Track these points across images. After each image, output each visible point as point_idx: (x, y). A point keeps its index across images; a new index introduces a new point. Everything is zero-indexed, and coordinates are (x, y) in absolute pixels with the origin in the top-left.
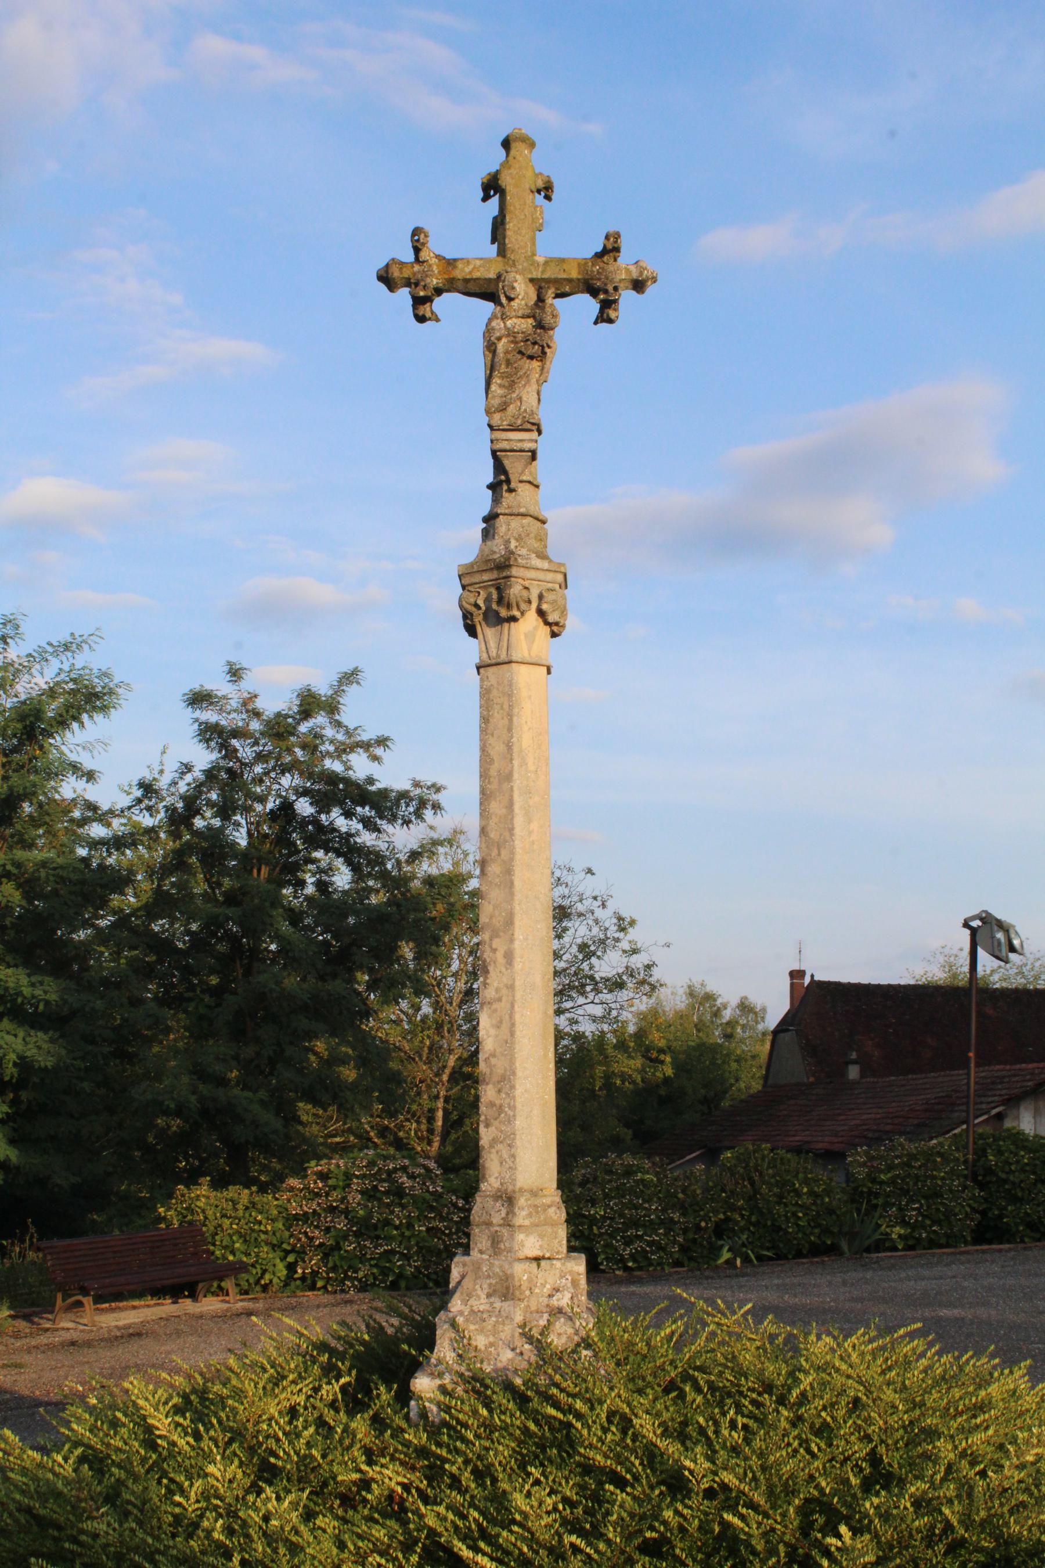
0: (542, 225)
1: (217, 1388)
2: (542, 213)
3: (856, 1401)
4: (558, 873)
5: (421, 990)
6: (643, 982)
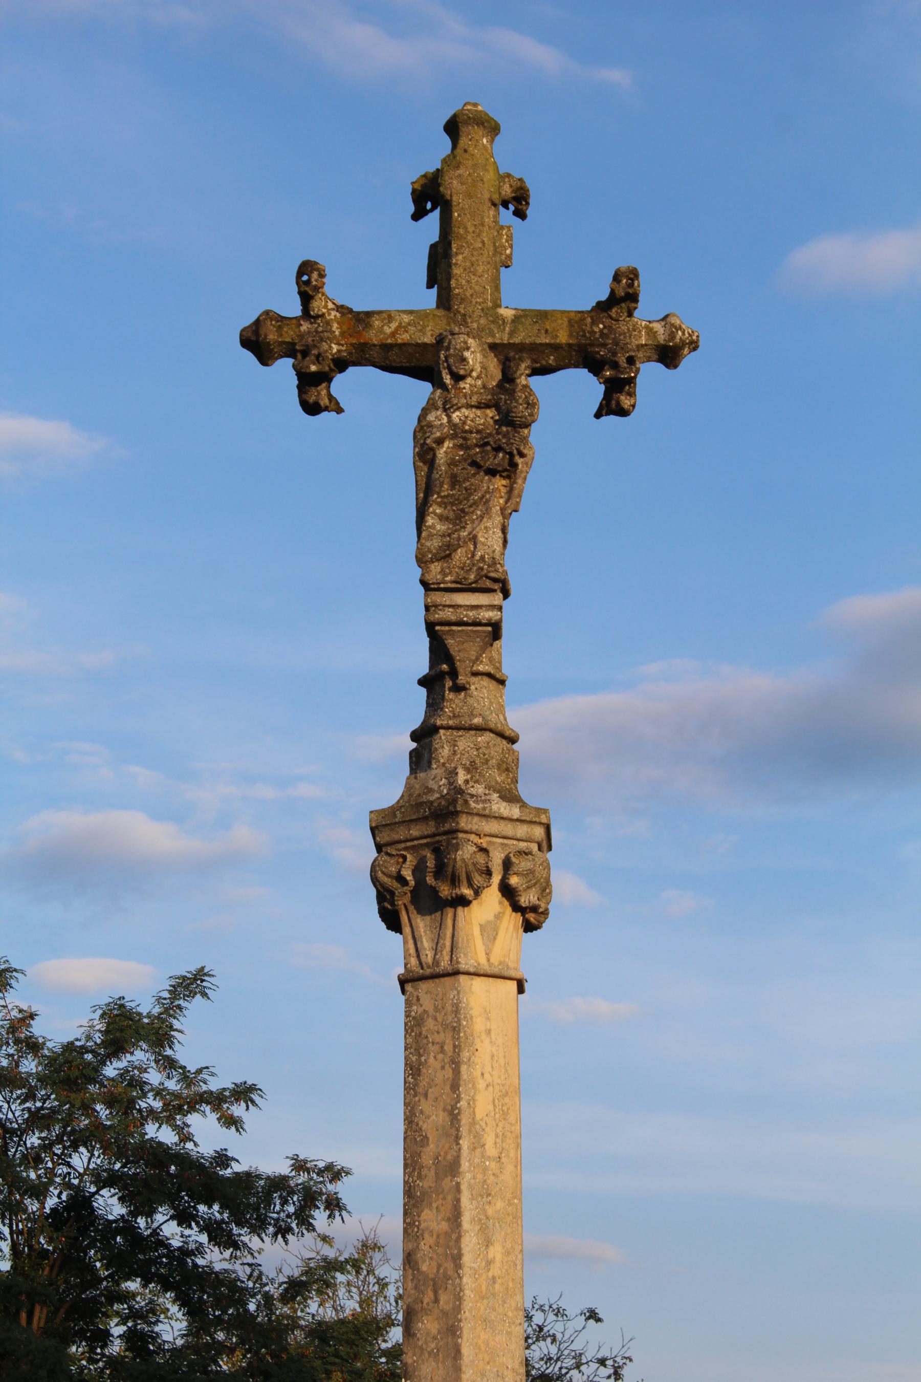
0: (509, 257)
2: (510, 238)
4: (538, 1318)
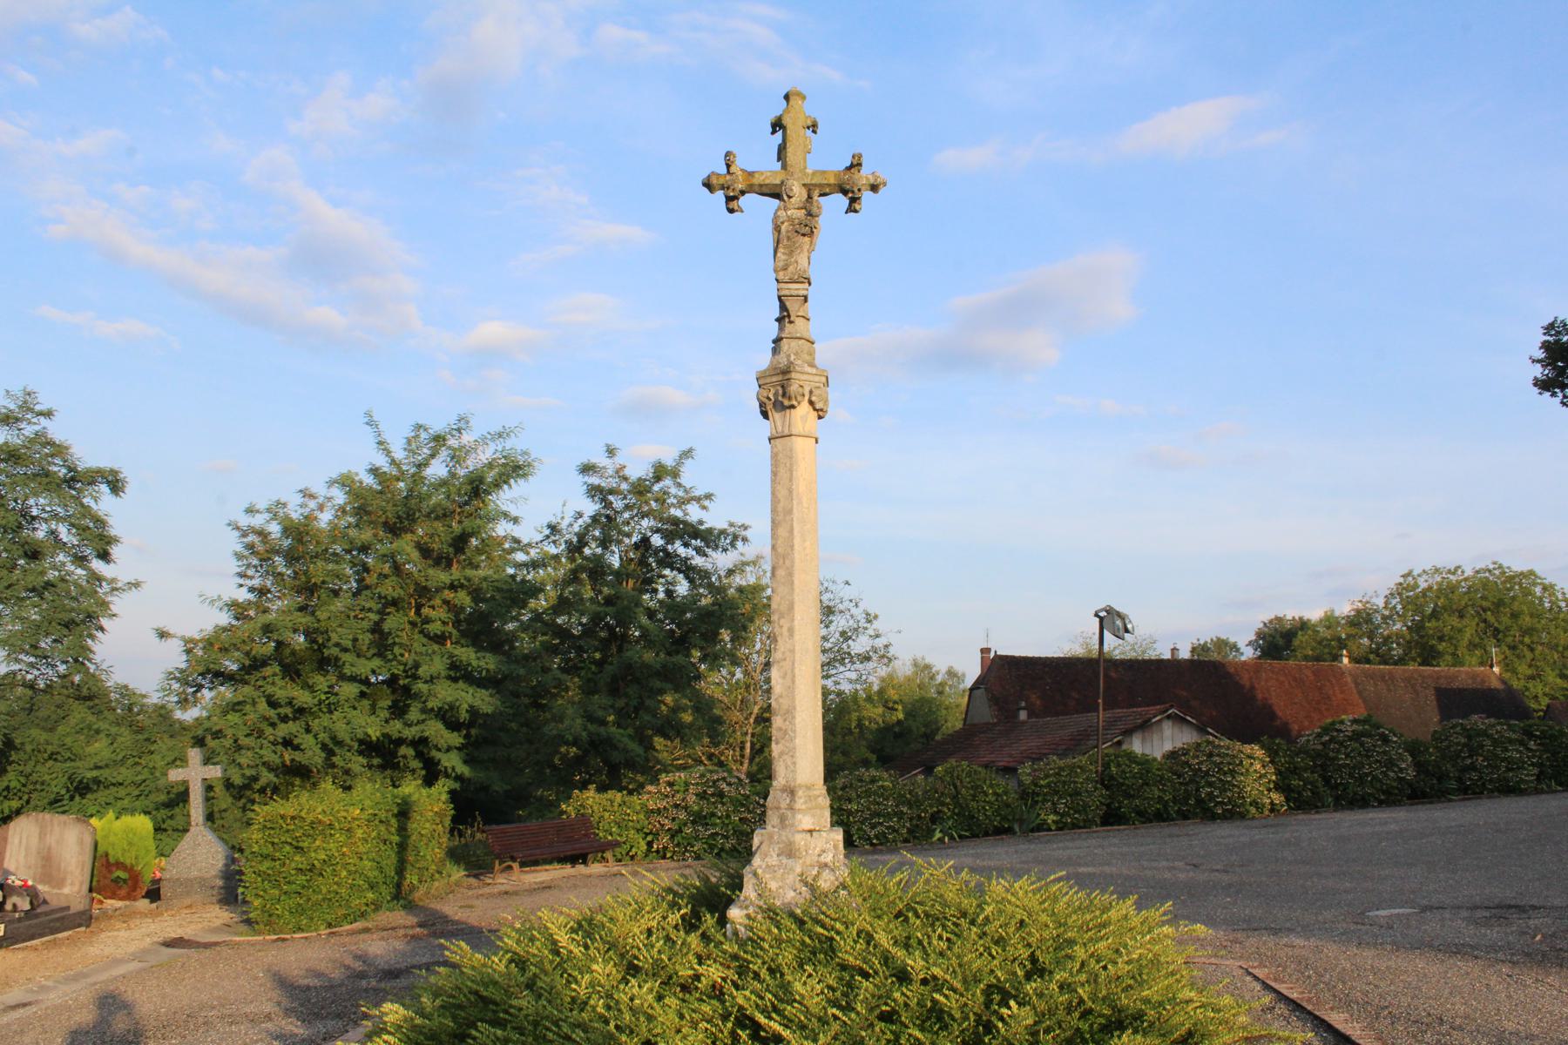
1: (599, 917)
3: (1022, 921)
5: (735, 662)
6: (883, 657)
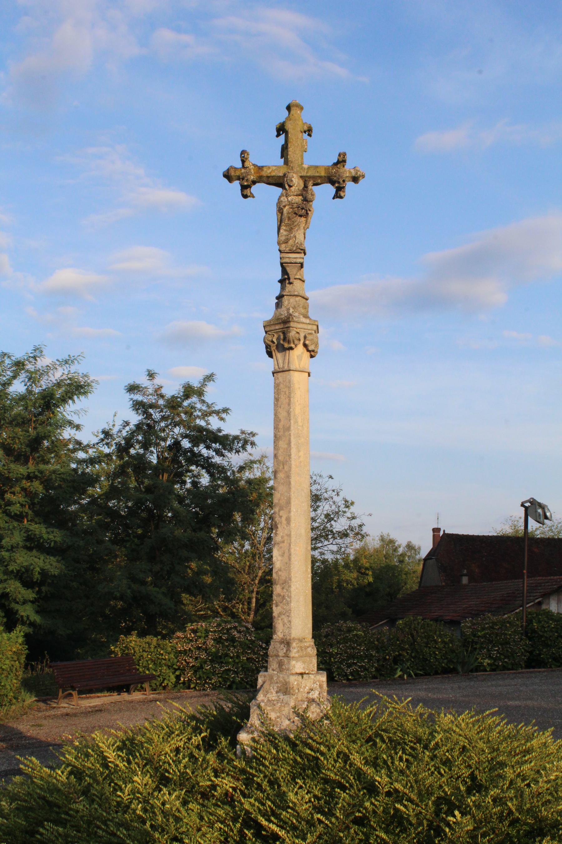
0: (306, 149)
2: (306, 143)
4: (314, 478)
